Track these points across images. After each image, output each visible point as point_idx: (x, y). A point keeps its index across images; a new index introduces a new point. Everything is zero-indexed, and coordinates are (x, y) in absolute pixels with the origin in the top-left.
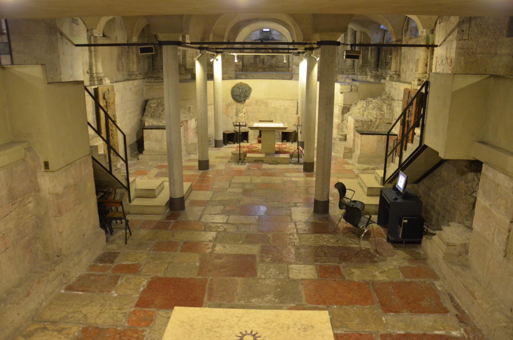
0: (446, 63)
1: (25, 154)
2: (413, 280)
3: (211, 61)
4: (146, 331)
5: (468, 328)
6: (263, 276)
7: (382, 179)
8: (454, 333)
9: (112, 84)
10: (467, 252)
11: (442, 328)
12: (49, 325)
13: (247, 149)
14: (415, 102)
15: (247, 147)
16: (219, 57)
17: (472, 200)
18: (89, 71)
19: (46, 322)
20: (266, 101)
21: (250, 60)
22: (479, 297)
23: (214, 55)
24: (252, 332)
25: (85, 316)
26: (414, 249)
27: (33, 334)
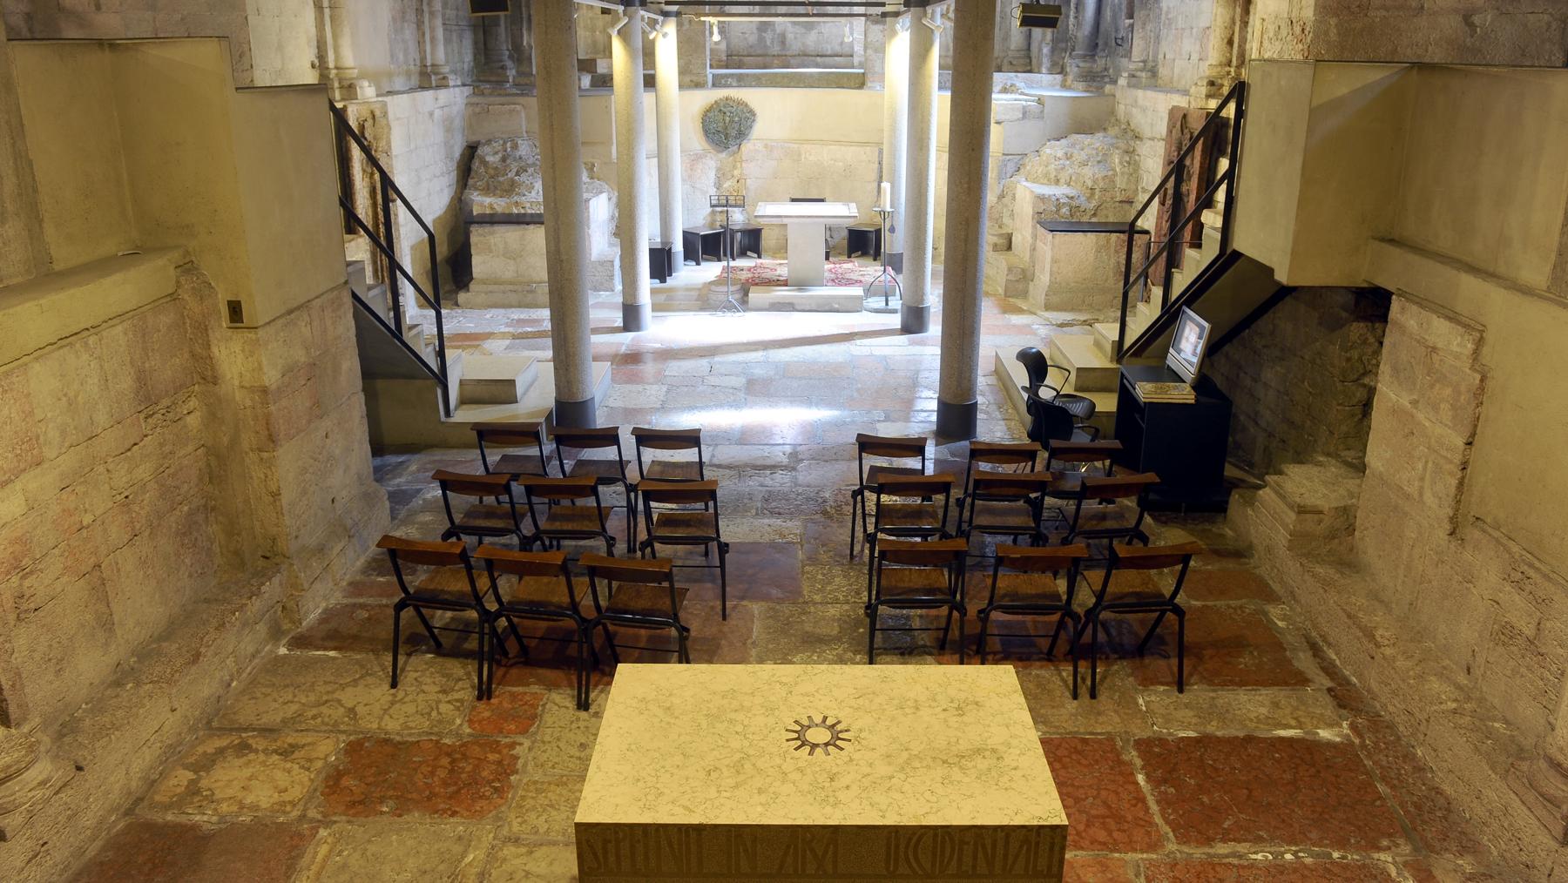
1: (178, 282)
2: (1209, 603)
3: (651, 37)
4: (521, 744)
5: (1360, 720)
6: (817, 598)
7: (1116, 344)
8: (1325, 734)
9: (380, 99)
10: (1351, 529)
11: (1293, 723)
12: (253, 737)
13: (750, 275)
14: (1199, 146)
15: (749, 270)
16: (671, 28)
17: (1360, 394)
18: (317, 62)
19: (246, 730)
20: (796, 146)
22: (1386, 642)
23: (656, 22)
24: (825, 718)
25: (352, 711)
26: (1207, 526)
27: (214, 762)
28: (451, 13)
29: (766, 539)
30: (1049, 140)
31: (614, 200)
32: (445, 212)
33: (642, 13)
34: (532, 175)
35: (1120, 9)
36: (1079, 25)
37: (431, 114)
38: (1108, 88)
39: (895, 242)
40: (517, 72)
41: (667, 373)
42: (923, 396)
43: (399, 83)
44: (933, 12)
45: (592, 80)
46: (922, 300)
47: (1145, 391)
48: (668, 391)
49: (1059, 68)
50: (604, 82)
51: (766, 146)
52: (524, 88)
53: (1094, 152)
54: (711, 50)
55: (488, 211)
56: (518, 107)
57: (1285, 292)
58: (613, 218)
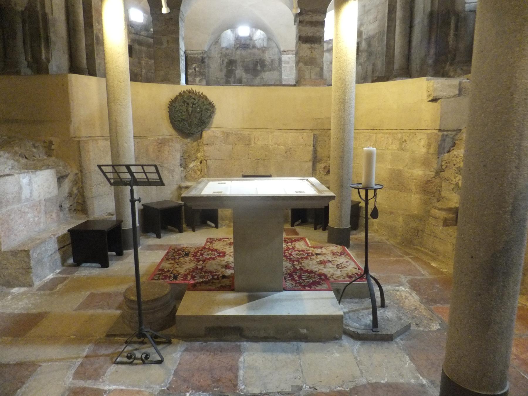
21: (219, 80)
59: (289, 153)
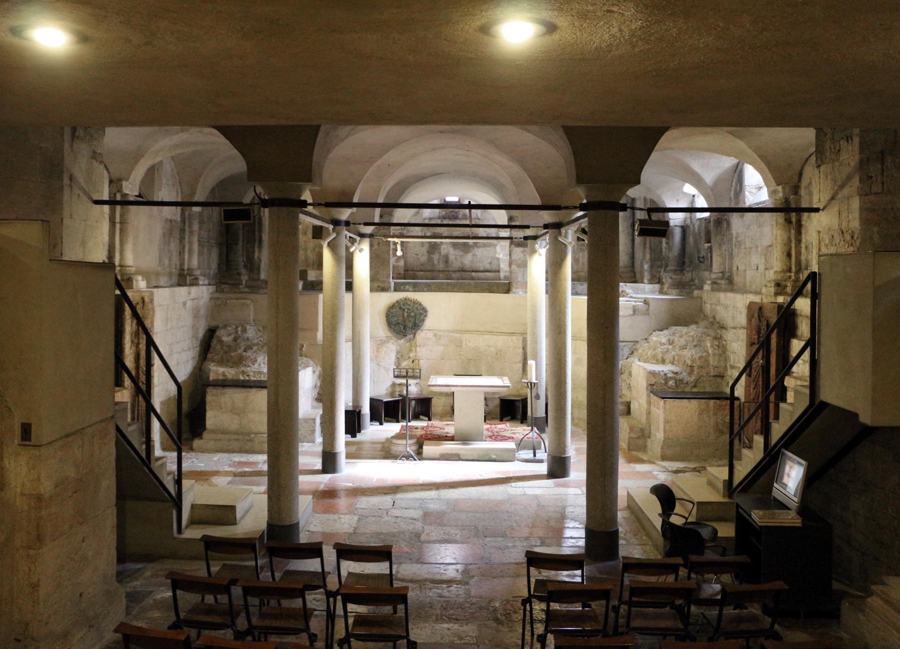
0: (841, 240)
3: (351, 250)
9: (149, 290)
13: (423, 432)
21: (419, 256)
28: (204, 234)
29: (447, 640)
30: (654, 331)
31: (317, 373)
32: (188, 378)
33: (346, 232)
34: (256, 352)
35: (700, 236)
36: (670, 248)
37: (185, 304)
38: (696, 292)
39: (537, 409)
40: (249, 278)
41: (357, 506)
42: (571, 526)
43: (163, 281)
44: (566, 233)
45: (307, 275)
46: (564, 452)
47: (758, 517)
48: (359, 520)
49: (656, 279)
50: (313, 286)
51: (435, 335)
52: (256, 286)
53: (691, 339)
54: (394, 267)
55: (221, 378)
56: (248, 302)
57: (867, 432)
58: (316, 386)
59: (499, 355)
